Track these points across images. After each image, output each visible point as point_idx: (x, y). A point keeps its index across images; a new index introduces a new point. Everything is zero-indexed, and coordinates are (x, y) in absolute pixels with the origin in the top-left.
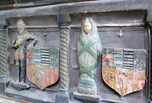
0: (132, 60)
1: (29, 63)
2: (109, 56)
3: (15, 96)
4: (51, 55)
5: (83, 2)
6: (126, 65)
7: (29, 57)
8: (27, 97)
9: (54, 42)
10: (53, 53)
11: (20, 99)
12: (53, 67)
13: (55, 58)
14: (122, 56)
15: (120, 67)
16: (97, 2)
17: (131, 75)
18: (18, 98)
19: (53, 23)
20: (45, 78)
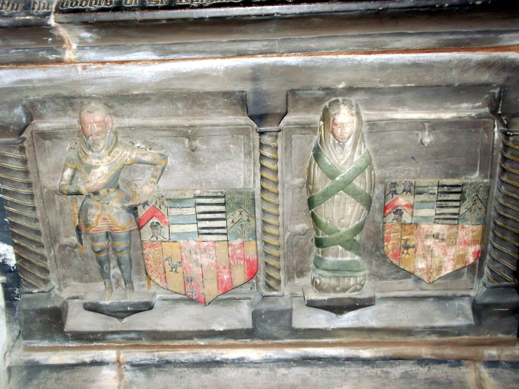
0: (457, 204)
1: (154, 239)
2: (402, 201)
3: (109, 337)
4: (233, 210)
5: (335, 57)
6: (442, 217)
7: (151, 221)
8: (156, 332)
9: (226, 167)
10: (239, 205)
11: (132, 339)
12: (239, 241)
13: (245, 218)
14: (433, 198)
15: (427, 221)
16: (376, 59)
17: (452, 237)
18: (123, 338)
19: (221, 113)
20: (215, 274)
